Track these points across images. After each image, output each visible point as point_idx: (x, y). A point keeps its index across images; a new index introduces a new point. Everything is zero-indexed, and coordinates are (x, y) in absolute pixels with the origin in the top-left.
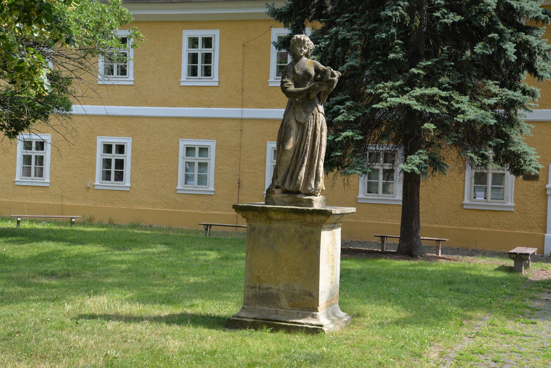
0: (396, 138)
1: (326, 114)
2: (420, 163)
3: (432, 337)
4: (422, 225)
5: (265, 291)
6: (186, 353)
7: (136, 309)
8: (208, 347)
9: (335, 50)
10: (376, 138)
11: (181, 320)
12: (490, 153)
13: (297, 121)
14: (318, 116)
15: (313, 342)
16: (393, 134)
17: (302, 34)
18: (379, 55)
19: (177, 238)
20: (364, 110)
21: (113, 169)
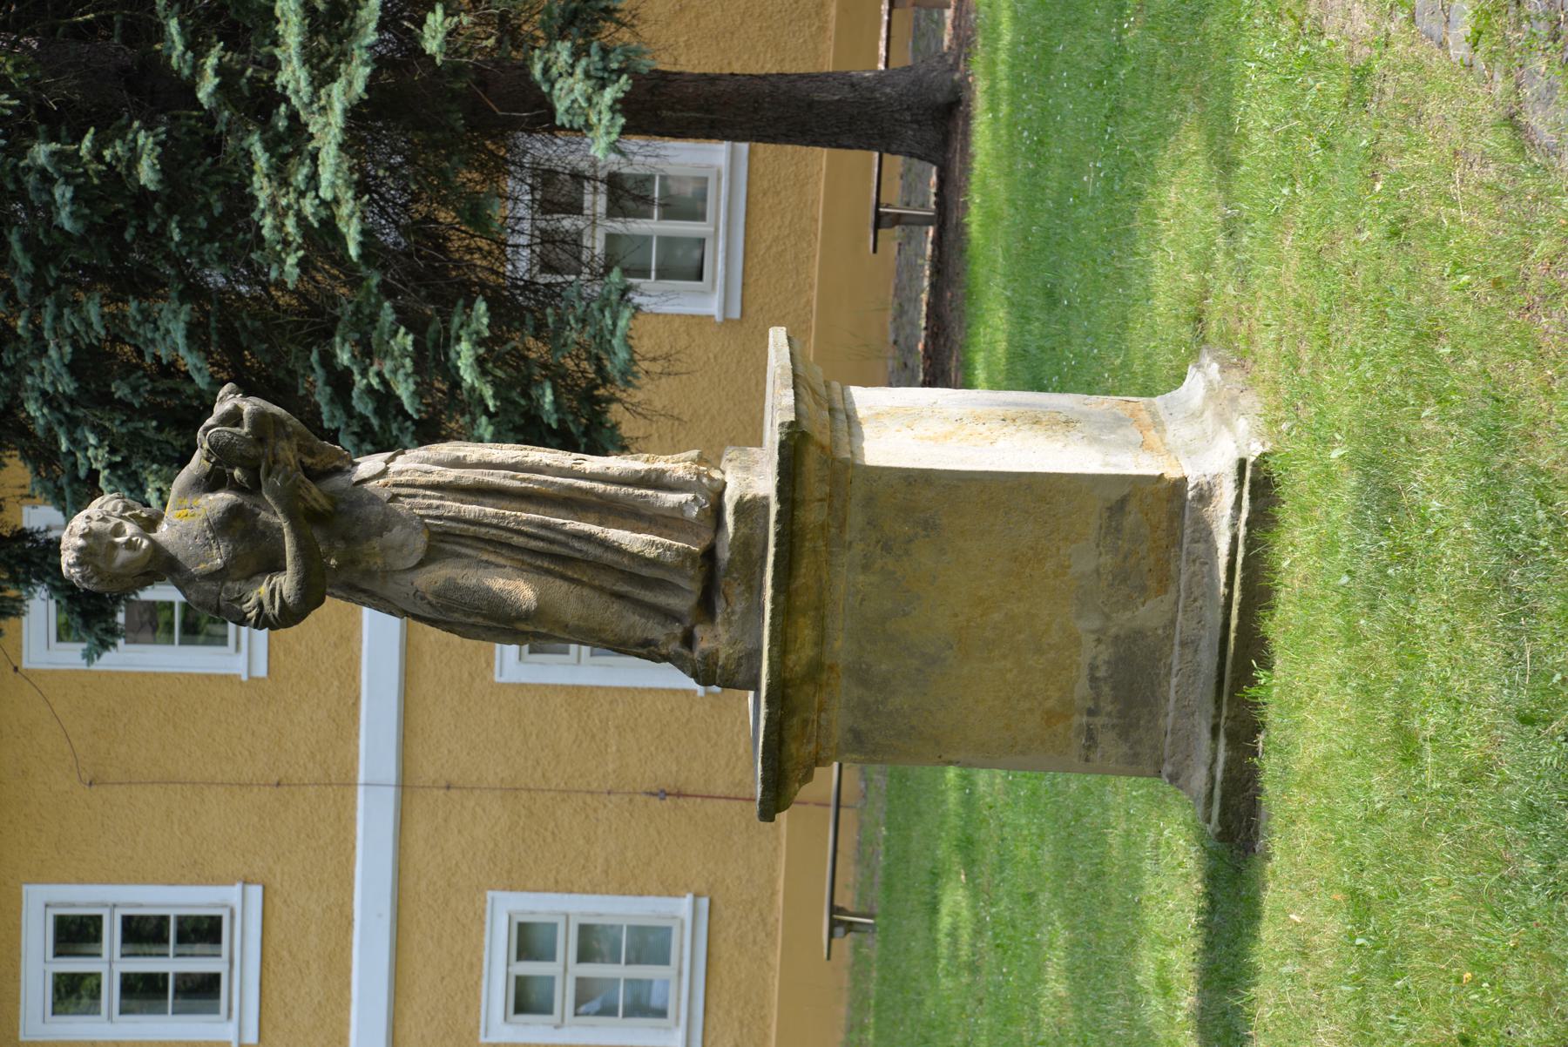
0: (482, 167)
2: (587, 75)
3: (1286, 27)
4: (828, 64)
5: (1106, 689)
6: (1364, 1015)
8: (1336, 925)
9: (123, 405)
10: (483, 244)
13: (421, 564)
14: (403, 479)
15: (1306, 498)
16: (465, 175)
17: (58, 542)
18: (142, 228)
20: (369, 292)
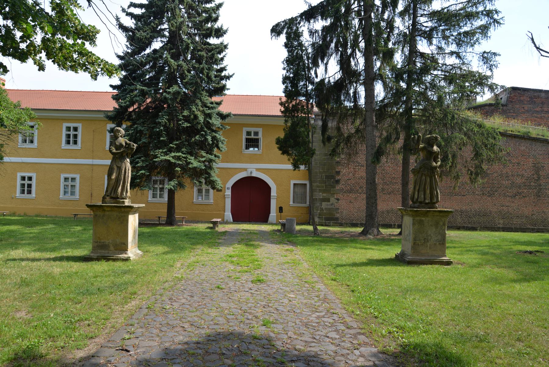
1: (131, 163)
7: (37, 255)
8: (74, 270)
11: (61, 259)
12: (203, 181)
19: (57, 221)
21: (26, 189)
